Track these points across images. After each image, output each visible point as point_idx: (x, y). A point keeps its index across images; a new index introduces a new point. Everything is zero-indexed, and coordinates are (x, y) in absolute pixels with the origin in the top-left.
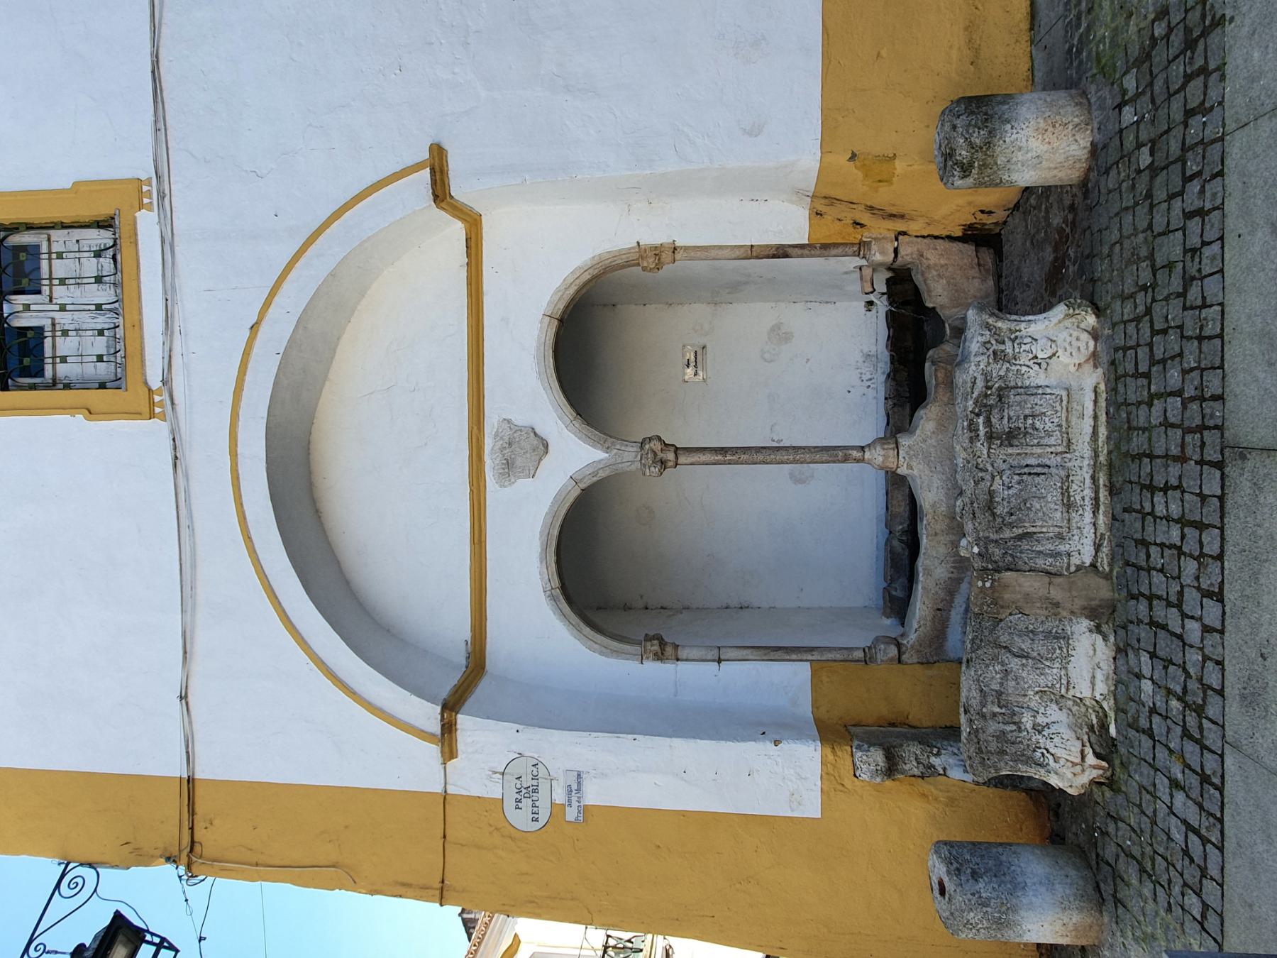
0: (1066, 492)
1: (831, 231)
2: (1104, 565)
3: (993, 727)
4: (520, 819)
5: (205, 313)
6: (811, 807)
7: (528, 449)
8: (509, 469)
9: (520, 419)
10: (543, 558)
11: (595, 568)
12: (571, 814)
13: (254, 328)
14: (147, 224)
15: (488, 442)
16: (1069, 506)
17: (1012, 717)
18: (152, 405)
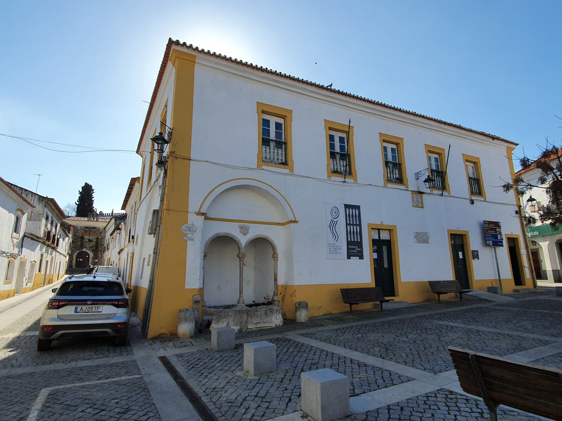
0: (258, 323)
1: (280, 289)
2: (248, 330)
3: (223, 314)
4: (184, 227)
5: (272, 176)
6: (187, 287)
7: (245, 231)
8: (241, 228)
9: (250, 230)
10: (225, 233)
11: (221, 242)
12: (185, 238)
13: (271, 186)
14: (287, 171)
15: (246, 224)
16: (256, 324)
17: (224, 317)
18: (259, 166)
